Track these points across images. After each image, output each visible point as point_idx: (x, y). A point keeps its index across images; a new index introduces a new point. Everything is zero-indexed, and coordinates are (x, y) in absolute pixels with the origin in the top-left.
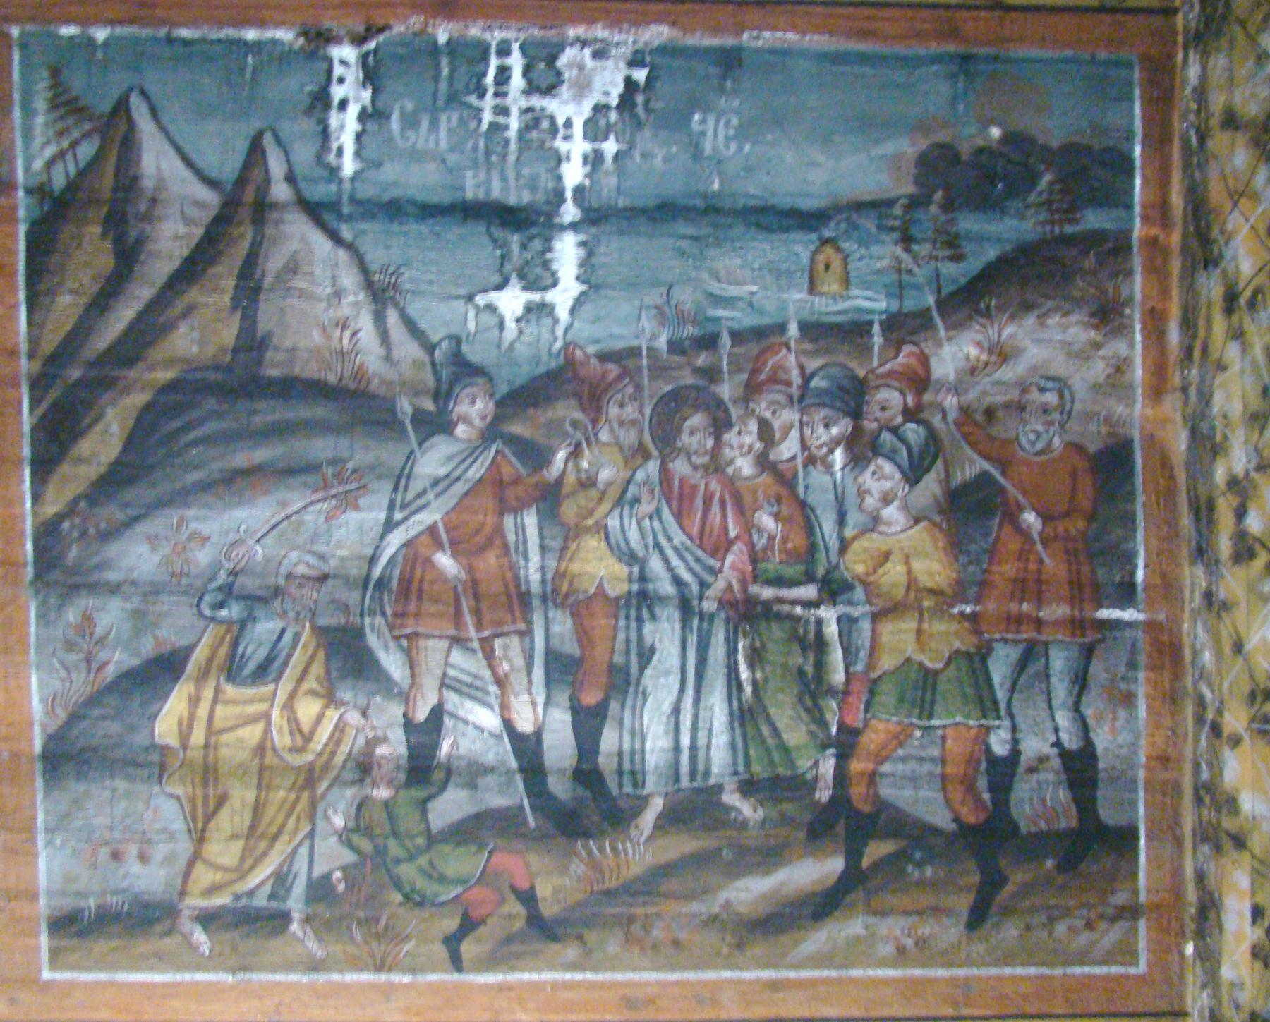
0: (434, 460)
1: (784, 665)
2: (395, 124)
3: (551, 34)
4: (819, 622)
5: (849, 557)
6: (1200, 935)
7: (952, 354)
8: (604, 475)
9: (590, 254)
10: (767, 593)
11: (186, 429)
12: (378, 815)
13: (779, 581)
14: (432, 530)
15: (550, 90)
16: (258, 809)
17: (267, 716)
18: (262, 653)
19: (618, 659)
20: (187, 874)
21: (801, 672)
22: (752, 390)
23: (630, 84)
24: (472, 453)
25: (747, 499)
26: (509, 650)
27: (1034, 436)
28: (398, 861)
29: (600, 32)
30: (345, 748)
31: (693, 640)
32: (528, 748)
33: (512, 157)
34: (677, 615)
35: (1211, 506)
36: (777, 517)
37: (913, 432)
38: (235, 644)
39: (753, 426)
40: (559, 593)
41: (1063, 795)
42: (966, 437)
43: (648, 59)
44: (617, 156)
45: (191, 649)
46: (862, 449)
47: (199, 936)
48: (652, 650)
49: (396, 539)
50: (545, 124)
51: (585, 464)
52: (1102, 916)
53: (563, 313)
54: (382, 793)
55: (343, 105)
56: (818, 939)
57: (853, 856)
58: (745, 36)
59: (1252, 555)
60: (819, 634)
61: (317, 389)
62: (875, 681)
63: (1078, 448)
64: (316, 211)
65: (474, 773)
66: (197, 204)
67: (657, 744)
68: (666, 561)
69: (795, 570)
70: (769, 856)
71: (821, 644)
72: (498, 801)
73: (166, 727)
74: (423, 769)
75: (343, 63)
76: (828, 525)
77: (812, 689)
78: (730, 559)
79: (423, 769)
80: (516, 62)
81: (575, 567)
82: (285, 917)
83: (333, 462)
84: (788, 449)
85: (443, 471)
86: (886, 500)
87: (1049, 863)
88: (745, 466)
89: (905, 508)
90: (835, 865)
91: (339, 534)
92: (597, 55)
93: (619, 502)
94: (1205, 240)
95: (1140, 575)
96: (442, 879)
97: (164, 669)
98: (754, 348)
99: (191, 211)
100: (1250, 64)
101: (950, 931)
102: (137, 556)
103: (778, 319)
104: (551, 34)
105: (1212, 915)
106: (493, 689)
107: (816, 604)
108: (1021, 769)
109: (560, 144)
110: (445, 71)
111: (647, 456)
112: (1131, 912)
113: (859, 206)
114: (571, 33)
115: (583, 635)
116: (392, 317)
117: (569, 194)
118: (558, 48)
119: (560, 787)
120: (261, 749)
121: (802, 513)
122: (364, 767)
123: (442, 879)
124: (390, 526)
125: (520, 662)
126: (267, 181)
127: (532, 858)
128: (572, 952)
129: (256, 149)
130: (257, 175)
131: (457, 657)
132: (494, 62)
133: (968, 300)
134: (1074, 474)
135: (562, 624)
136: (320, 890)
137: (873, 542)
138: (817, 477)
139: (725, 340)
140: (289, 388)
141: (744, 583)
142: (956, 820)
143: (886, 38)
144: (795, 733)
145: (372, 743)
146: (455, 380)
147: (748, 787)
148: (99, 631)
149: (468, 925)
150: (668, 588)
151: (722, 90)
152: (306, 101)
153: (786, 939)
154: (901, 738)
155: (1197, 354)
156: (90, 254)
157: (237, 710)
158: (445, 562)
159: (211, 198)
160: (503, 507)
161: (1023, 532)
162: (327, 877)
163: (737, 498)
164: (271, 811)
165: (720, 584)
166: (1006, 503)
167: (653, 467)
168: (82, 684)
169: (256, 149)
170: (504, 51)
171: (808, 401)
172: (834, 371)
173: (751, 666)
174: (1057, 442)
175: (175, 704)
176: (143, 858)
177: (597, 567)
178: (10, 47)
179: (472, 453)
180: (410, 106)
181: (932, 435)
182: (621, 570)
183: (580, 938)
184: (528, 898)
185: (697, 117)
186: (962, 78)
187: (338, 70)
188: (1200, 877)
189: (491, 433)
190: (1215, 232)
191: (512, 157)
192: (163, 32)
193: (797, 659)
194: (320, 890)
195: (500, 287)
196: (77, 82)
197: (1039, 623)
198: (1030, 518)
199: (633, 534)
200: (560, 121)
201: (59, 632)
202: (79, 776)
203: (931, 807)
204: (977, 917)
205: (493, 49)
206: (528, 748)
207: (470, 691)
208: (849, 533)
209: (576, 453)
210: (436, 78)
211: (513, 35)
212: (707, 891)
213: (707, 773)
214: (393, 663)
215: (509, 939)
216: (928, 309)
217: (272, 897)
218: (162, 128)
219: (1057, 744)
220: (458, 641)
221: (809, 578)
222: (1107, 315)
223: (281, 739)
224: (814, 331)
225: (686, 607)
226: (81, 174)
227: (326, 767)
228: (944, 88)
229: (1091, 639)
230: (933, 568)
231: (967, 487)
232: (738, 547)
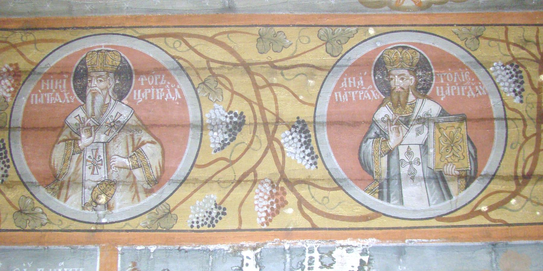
3: (330, 245)
29: (349, 242)
43: (368, 252)
58: (407, 241)
75: (248, 257)
80: (316, 255)
92: (348, 251)
104: (330, 245)
110: (288, 260)
132: (308, 255)
143: (462, 240)
151: (398, 263)
170: (311, 251)
178: (117, 254)
186: (493, 254)
187: (246, 261)
192: (177, 247)
205: (307, 251)
210: (285, 263)
228: (487, 258)
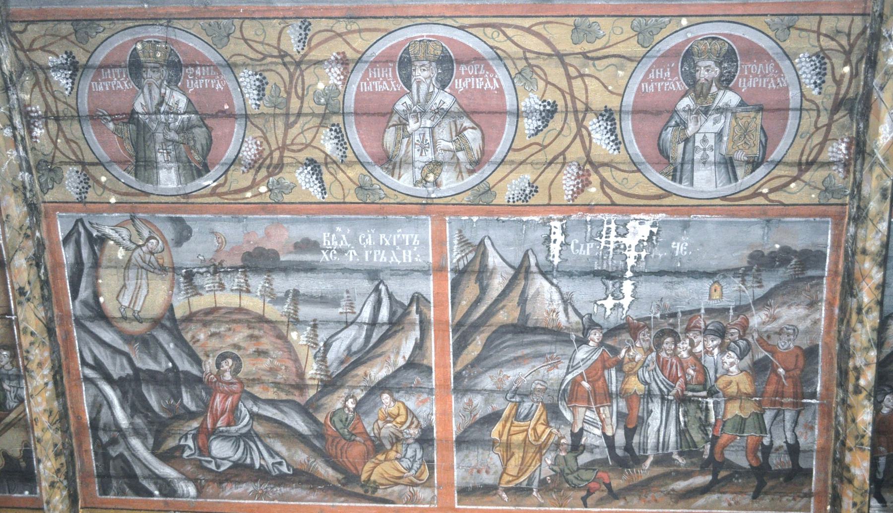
0: (582, 353)
1: (695, 417)
2: (572, 247)
3: (626, 218)
4: (707, 403)
5: (718, 383)
6: (833, 505)
7: (757, 319)
8: (638, 357)
9: (636, 287)
10: (690, 394)
11: (504, 342)
12: (562, 461)
13: (693, 390)
14: (581, 374)
15: (624, 236)
16: (523, 458)
17: (527, 430)
18: (526, 412)
19: (640, 414)
20: (500, 478)
21: (700, 418)
22: (688, 330)
23: (651, 233)
24: (595, 350)
25: (685, 365)
26: (605, 411)
27: (783, 344)
28: (568, 474)
29: (641, 216)
30: (551, 441)
31: (665, 408)
32: (610, 441)
33: (611, 257)
34: (660, 401)
35: (847, 373)
36: (694, 370)
37: (742, 343)
38: (517, 410)
39: (688, 341)
40: (622, 394)
41: (787, 458)
42: (760, 344)
44: (645, 257)
45: (504, 410)
46: (724, 349)
47: (504, 495)
48: (652, 411)
49: (570, 377)
50: (622, 247)
51: (631, 354)
52: (799, 496)
53: (626, 307)
54: (563, 454)
55: (555, 241)
56: (701, 501)
57: (715, 475)
59: (861, 392)
60: (707, 407)
61: (545, 331)
62: (725, 422)
63: (799, 347)
64: (544, 274)
65: (592, 449)
66: (507, 273)
67: (651, 441)
68: (657, 384)
69: (698, 387)
70: (687, 475)
71: (707, 409)
72: (598, 457)
73: (495, 435)
74: (577, 447)
76: (712, 373)
77: (704, 425)
78: (678, 383)
79: (577, 447)
80: (613, 226)
81: (627, 386)
82: (531, 490)
83: (550, 353)
84: (699, 348)
85: (585, 356)
86: (732, 364)
87: (781, 479)
88: (685, 354)
89: (738, 368)
90: (709, 478)
91: (551, 376)
92: (640, 223)
93: (642, 366)
94: (852, 288)
95: (818, 389)
96: (582, 480)
97: (492, 418)
98: (690, 317)
99: (506, 276)
100: (874, 233)
101: (746, 499)
102: (487, 382)
103: (697, 307)
104: (626, 218)
105: (838, 502)
106: (600, 423)
107: (706, 398)
108: (773, 450)
109: (626, 252)
110: (589, 230)
111: (652, 351)
112: (809, 495)
113: (727, 270)
114: (633, 216)
115: (630, 408)
116: (570, 309)
117: (629, 268)
118: (628, 221)
119: (619, 452)
120: (525, 440)
121: (704, 370)
122: (558, 445)
123: (582, 480)
124: (567, 373)
125: (608, 415)
126: (529, 266)
127: (610, 474)
128: (622, 503)
129: (526, 255)
130: (526, 264)
131: (588, 413)
132: (606, 226)
133: (762, 302)
134: (797, 356)
135: (622, 404)
136: (543, 482)
137: (726, 378)
138: (709, 358)
139: (680, 315)
140: (535, 330)
141: (682, 391)
142: (750, 465)
144: (697, 436)
145: (560, 438)
146: (590, 328)
147: (681, 454)
148: (474, 405)
149: (590, 493)
150: (657, 392)
152: (543, 240)
153: (691, 500)
154: (733, 439)
155: (845, 322)
156: (471, 290)
157: (517, 429)
158: (585, 384)
159: (512, 272)
160: (604, 368)
161: (778, 375)
162: (545, 479)
163: (681, 364)
164: (527, 459)
165: (674, 392)
166: (773, 365)
167: (654, 354)
168: (468, 421)
169: (526, 255)
170: (609, 222)
171: (707, 332)
172: (716, 324)
173: (684, 416)
174: (792, 346)
175: (498, 427)
176: (487, 472)
177: (635, 385)
179: (595, 350)
180: (577, 241)
181: (748, 343)
182: (642, 387)
183: (625, 498)
184: (608, 486)
185: (674, 243)
187: (553, 230)
188: (834, 488)
189: (601, 344)
190: (855, 286)
191: (611, 257)
192: (496, 218)
193: (699, 414)
194: (543, 482)
195: (605, 299)
196: (467, 235)
197: (782, 404)
198: (781, 370)
199: (647, 375)
200: (627, 246)
201: (461, 405)
202: (467, 448)
203: (742, 461)
204: (755, 497)
206: (610, 441)
207: (592, 424)
208: (718, 376)
209: (628, 350)
210: (586, 232)
211: (613, 217)
212: (667, 484)
213: (668, 448)
214: (568, 415)
215: (601, 499)
216: (749, 304)
217: (528, 484)
218: (495, 249)
219: (786, 442)
220: (589, 408)
221: (705, 389)
222: (813, 304)
223: (531, 438)
224: (709, 311)
225: (663, 399)
226: (469, 263)
227: (546, 445)
228: (760, 232)
229: (799, 408)
230: (746, 386)
231: (760, 360)
232: (681, 380)
